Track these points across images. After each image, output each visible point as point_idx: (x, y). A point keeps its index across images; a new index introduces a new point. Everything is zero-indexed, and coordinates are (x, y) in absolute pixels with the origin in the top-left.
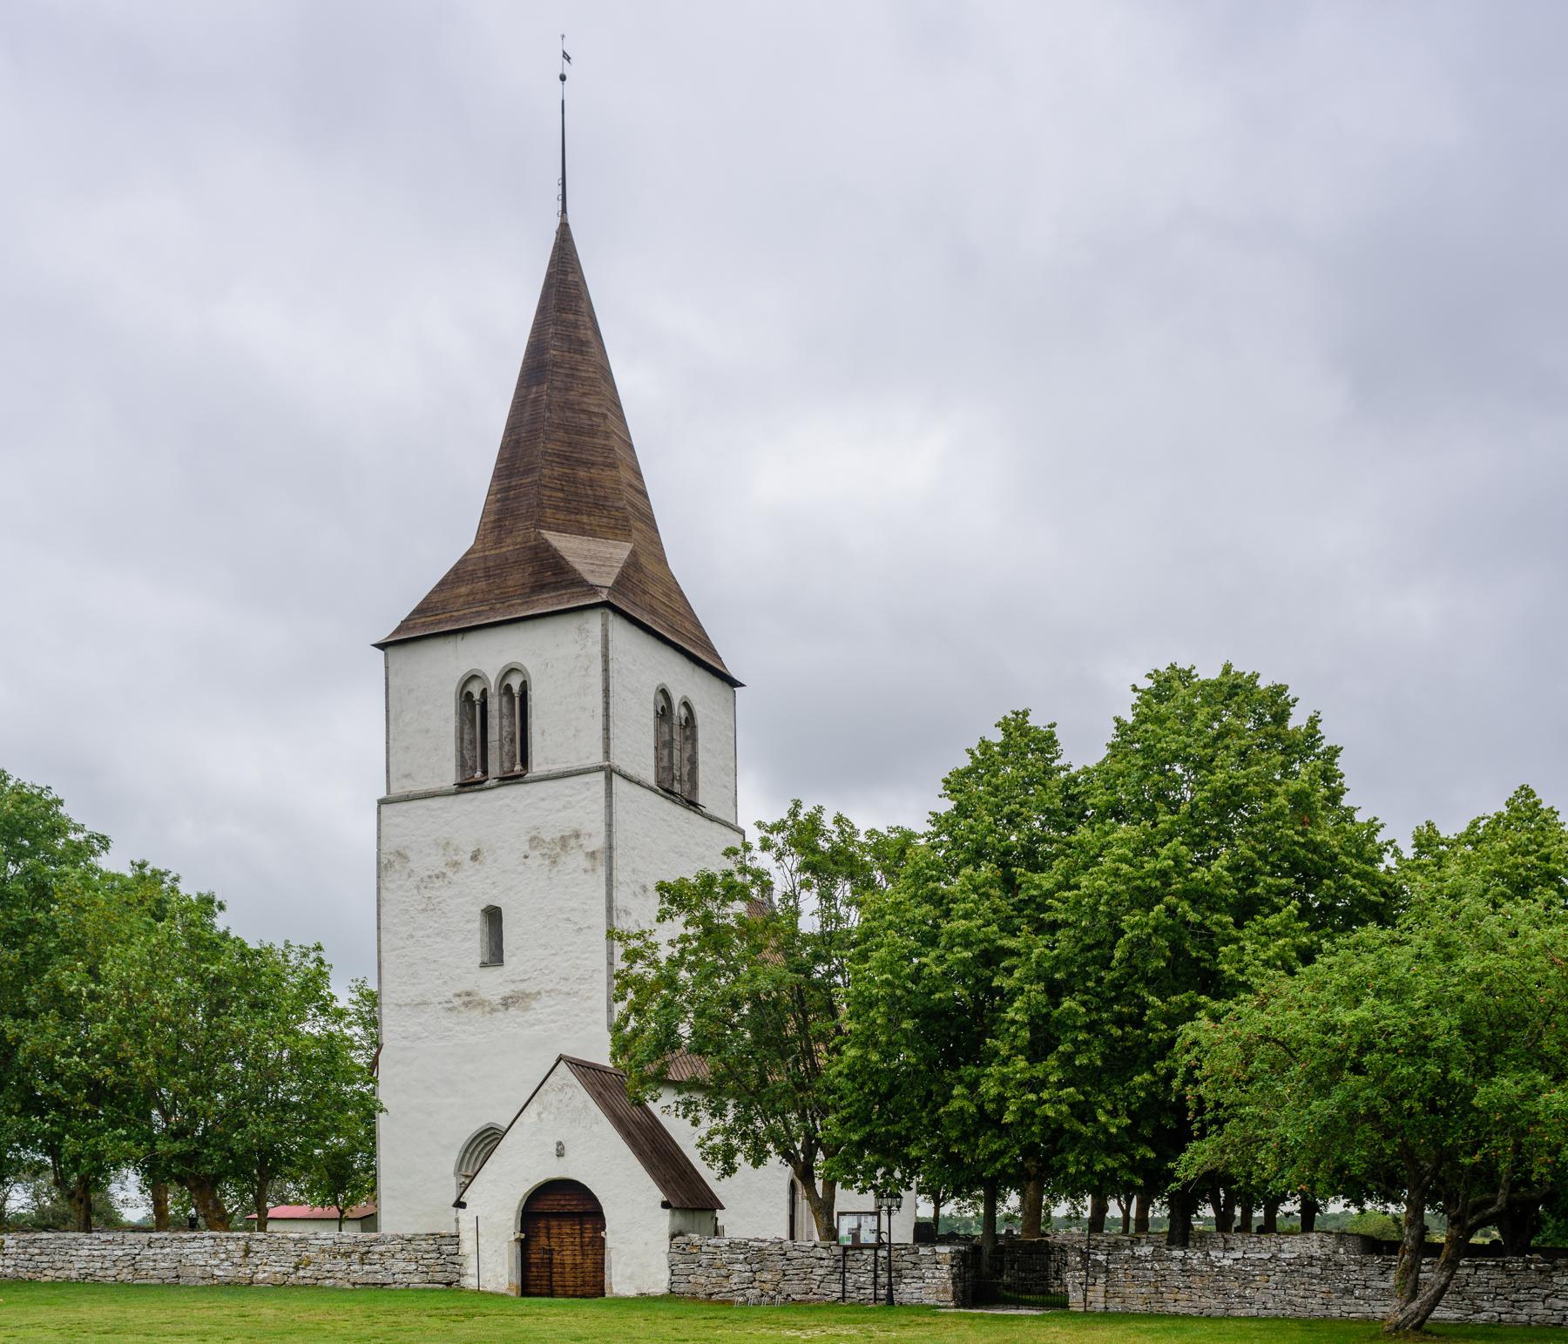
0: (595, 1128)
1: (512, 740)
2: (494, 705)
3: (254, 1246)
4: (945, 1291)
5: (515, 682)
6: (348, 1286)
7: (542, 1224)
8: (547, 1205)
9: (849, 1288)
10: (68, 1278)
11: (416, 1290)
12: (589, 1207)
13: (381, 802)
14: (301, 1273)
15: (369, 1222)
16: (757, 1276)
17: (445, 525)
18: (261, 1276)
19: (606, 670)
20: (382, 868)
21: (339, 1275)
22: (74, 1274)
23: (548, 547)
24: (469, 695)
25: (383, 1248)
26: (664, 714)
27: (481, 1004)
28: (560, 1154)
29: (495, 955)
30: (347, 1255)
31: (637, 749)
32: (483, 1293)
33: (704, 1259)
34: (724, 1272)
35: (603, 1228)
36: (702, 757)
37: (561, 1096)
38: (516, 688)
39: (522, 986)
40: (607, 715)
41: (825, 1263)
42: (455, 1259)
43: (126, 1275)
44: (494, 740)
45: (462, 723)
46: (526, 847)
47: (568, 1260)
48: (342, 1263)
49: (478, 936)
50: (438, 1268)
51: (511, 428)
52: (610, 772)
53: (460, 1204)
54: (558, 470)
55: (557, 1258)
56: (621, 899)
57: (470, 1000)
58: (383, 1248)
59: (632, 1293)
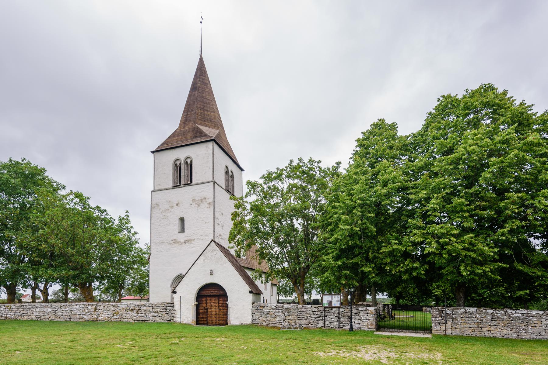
0: (225, 265)
1: (188, 176)
2: (183, 167)
3: (98, 307)
4: (372, 324)
5: (189, 161)
6: (132, 321)
7: (204, 299)
8: (207, 292)
9: (327, 323)
10: (32, 319)
11: (158, 323)
12: (222, 293)
13: (152, 191)
14: (115, 317)
15: (148, 300)
16: (287, 318)
17: (171, 125)
18: (100, 318)
19: (213, 157)
20: (152, 208)
21: (129, 317)
22: (34, 318)
23: (198, 128)
24: (176, 164)
25: (145, 308)
26: (227, 173)
27: (178, 242)
28: (211, 274)
29: (183, 230)
30: (132, 310)
31: (221, 179)
32: (183, 324)
33: (266, 311)
34: (273, 316)
35: (227, 300)
36: (235, 185)
37: (212, 254)
38: (189, 162)
39: (190, 238)
40: (213, 168)
41: (316, 313)
42: (172, 312)
43: (52, 318)
44: (183, 175)
45: (174, 172)
46: (191, 202)
47: (214, 312)
48: (130, 313)
49: (178, 225)
50: (166, 315)
51: (188, 101)
52: (214, 182)
53: (174, 292)
54: (200, 111)
55: (209, 311)
56: (217, 215)
57: (175, 241)
58: (145, 308)
59: (238, 323)
